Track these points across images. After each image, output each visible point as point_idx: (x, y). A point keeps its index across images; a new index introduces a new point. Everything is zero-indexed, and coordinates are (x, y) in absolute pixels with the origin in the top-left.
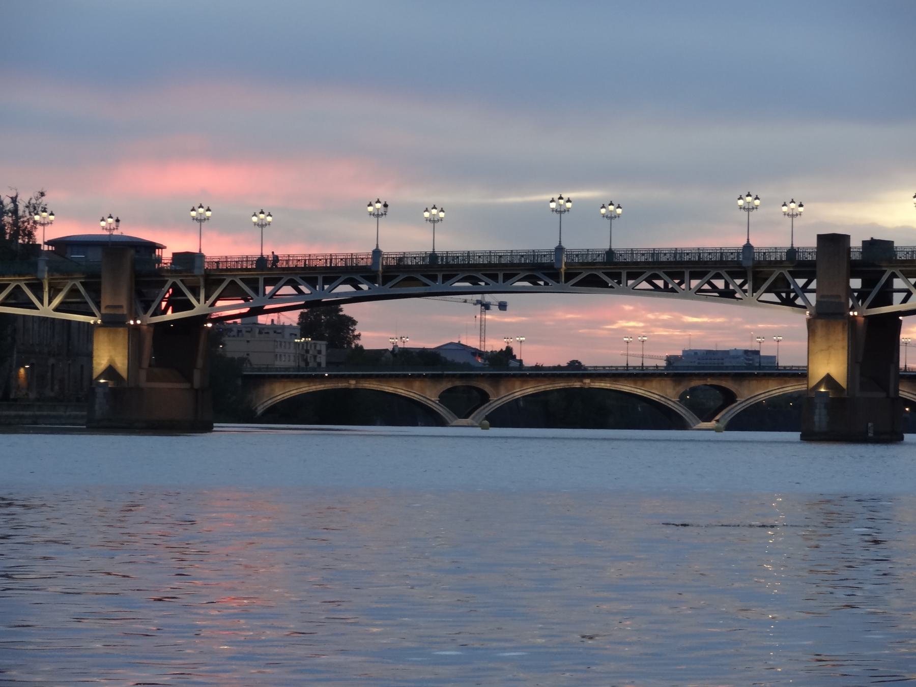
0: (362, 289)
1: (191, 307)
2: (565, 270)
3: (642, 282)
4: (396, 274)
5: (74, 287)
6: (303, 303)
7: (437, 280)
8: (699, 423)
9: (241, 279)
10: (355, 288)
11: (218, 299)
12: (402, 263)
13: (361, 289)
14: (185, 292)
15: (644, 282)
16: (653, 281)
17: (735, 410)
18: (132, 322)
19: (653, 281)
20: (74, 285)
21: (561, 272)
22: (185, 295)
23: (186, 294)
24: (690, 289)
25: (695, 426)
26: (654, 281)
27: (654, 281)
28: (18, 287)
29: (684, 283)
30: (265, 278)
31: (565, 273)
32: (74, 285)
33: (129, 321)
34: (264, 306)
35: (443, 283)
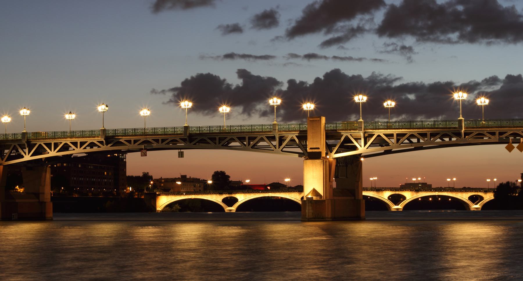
0: (445, 141)
1: (355, 148)
2: (464, 131)
3: (437, 139)
4: (473, 132)
5: (292, 139)
6: (413, 147)
7: (245, 140)
8: (227, 207)
9: (44, 143)
10: (441, 140)
11: (284, 147)
12: (18, 139)
13: (444, 140)
14: (352, 140)
15: (438, 139)
16: (443, 139)
17: (406, 202)
18: (24, 112)
19: (443, 139)
20: (292, 137)
21: (462, 132)
22: (353, 143)
23: (353, 141)
24: (394, 143)
25: (226, 208)
26: (229, 145)
27: (229, 145)
28: (15, 146)
29: (420, 139)
30: (249, 137)
31: (464, 133)
32: (292, 137)
33: (66, 165)
34: (392, 149)
35: (80, 148)
